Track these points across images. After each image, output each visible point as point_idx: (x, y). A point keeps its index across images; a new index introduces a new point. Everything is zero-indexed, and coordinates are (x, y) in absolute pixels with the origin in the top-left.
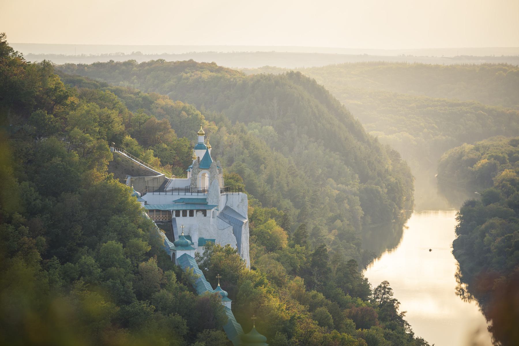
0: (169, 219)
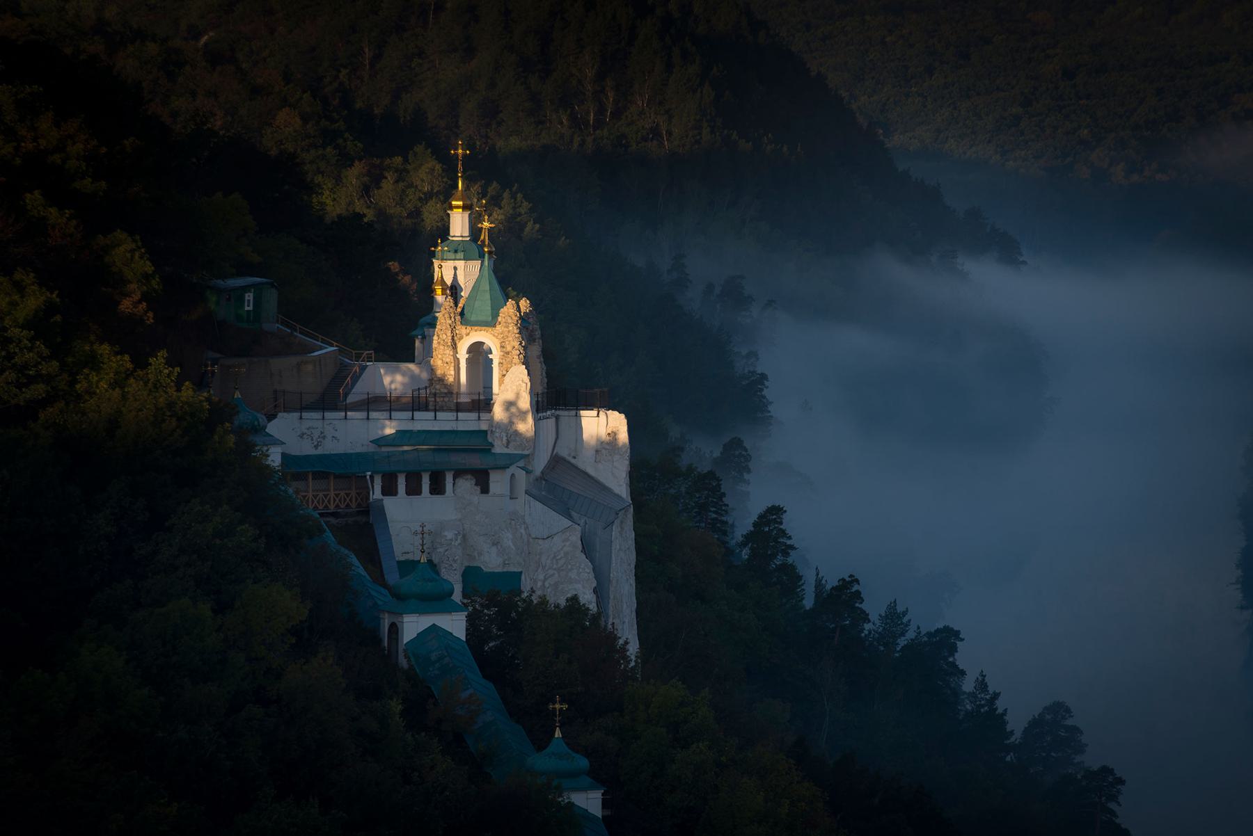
0: (359, 505)
